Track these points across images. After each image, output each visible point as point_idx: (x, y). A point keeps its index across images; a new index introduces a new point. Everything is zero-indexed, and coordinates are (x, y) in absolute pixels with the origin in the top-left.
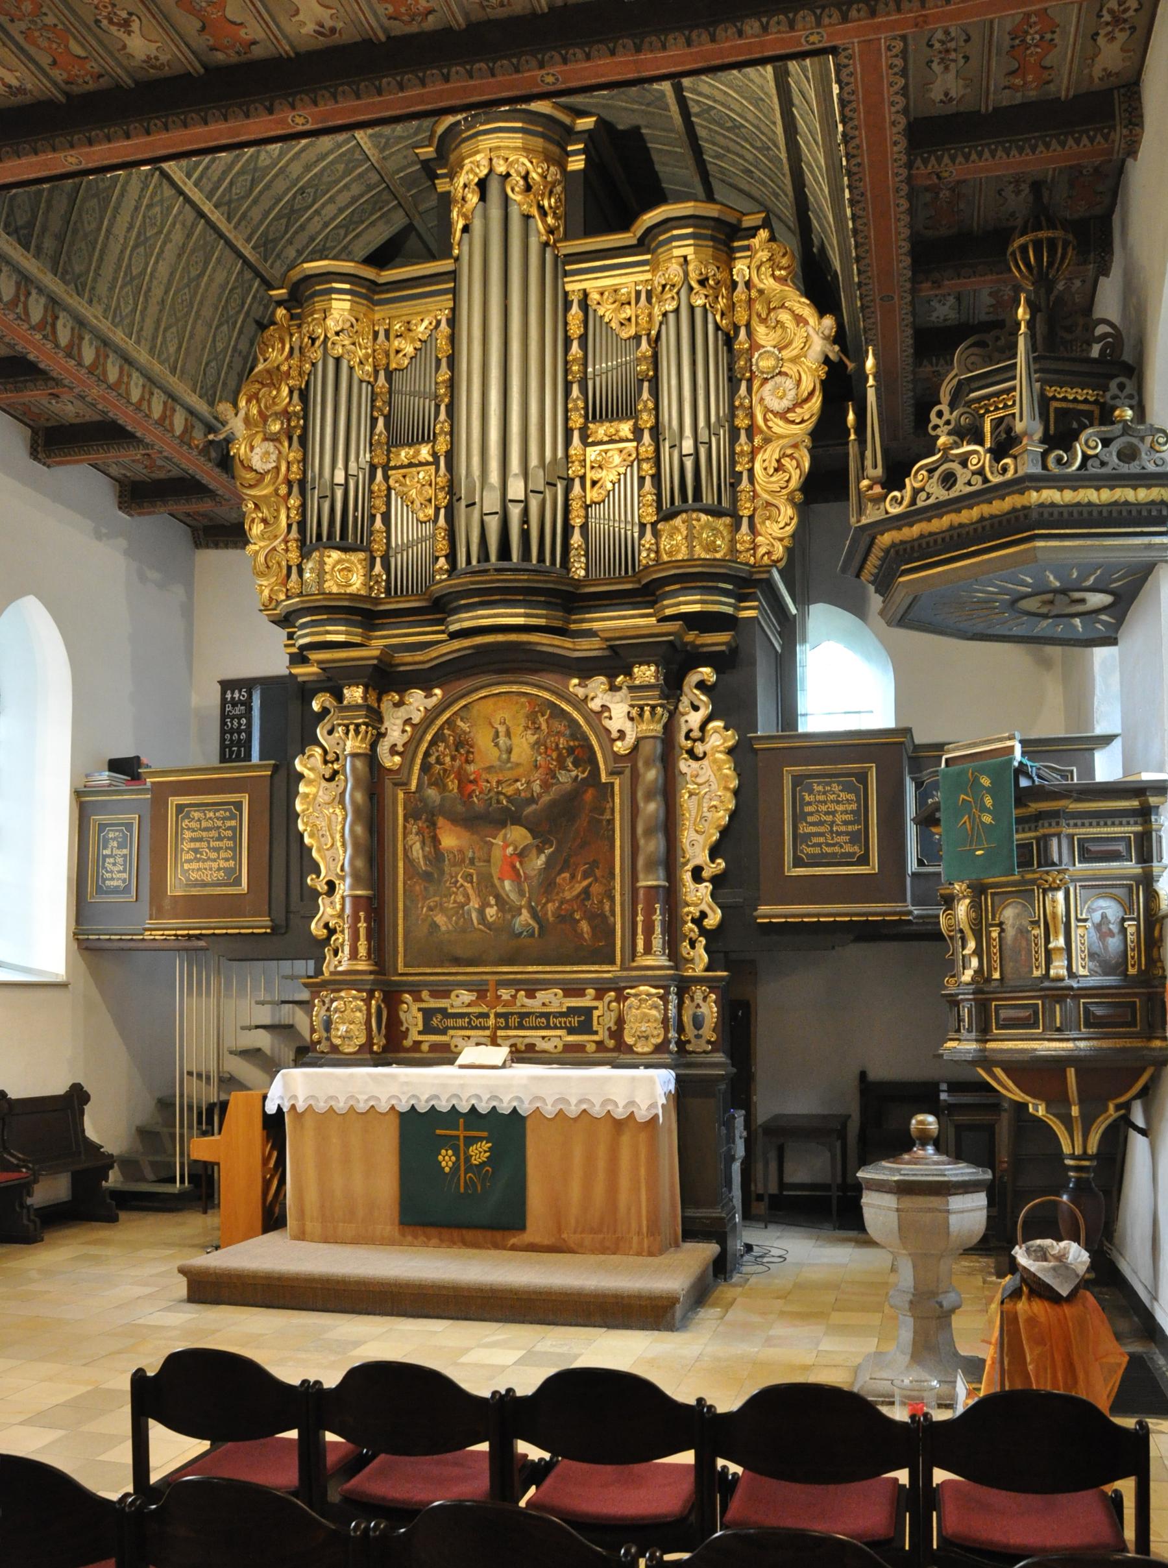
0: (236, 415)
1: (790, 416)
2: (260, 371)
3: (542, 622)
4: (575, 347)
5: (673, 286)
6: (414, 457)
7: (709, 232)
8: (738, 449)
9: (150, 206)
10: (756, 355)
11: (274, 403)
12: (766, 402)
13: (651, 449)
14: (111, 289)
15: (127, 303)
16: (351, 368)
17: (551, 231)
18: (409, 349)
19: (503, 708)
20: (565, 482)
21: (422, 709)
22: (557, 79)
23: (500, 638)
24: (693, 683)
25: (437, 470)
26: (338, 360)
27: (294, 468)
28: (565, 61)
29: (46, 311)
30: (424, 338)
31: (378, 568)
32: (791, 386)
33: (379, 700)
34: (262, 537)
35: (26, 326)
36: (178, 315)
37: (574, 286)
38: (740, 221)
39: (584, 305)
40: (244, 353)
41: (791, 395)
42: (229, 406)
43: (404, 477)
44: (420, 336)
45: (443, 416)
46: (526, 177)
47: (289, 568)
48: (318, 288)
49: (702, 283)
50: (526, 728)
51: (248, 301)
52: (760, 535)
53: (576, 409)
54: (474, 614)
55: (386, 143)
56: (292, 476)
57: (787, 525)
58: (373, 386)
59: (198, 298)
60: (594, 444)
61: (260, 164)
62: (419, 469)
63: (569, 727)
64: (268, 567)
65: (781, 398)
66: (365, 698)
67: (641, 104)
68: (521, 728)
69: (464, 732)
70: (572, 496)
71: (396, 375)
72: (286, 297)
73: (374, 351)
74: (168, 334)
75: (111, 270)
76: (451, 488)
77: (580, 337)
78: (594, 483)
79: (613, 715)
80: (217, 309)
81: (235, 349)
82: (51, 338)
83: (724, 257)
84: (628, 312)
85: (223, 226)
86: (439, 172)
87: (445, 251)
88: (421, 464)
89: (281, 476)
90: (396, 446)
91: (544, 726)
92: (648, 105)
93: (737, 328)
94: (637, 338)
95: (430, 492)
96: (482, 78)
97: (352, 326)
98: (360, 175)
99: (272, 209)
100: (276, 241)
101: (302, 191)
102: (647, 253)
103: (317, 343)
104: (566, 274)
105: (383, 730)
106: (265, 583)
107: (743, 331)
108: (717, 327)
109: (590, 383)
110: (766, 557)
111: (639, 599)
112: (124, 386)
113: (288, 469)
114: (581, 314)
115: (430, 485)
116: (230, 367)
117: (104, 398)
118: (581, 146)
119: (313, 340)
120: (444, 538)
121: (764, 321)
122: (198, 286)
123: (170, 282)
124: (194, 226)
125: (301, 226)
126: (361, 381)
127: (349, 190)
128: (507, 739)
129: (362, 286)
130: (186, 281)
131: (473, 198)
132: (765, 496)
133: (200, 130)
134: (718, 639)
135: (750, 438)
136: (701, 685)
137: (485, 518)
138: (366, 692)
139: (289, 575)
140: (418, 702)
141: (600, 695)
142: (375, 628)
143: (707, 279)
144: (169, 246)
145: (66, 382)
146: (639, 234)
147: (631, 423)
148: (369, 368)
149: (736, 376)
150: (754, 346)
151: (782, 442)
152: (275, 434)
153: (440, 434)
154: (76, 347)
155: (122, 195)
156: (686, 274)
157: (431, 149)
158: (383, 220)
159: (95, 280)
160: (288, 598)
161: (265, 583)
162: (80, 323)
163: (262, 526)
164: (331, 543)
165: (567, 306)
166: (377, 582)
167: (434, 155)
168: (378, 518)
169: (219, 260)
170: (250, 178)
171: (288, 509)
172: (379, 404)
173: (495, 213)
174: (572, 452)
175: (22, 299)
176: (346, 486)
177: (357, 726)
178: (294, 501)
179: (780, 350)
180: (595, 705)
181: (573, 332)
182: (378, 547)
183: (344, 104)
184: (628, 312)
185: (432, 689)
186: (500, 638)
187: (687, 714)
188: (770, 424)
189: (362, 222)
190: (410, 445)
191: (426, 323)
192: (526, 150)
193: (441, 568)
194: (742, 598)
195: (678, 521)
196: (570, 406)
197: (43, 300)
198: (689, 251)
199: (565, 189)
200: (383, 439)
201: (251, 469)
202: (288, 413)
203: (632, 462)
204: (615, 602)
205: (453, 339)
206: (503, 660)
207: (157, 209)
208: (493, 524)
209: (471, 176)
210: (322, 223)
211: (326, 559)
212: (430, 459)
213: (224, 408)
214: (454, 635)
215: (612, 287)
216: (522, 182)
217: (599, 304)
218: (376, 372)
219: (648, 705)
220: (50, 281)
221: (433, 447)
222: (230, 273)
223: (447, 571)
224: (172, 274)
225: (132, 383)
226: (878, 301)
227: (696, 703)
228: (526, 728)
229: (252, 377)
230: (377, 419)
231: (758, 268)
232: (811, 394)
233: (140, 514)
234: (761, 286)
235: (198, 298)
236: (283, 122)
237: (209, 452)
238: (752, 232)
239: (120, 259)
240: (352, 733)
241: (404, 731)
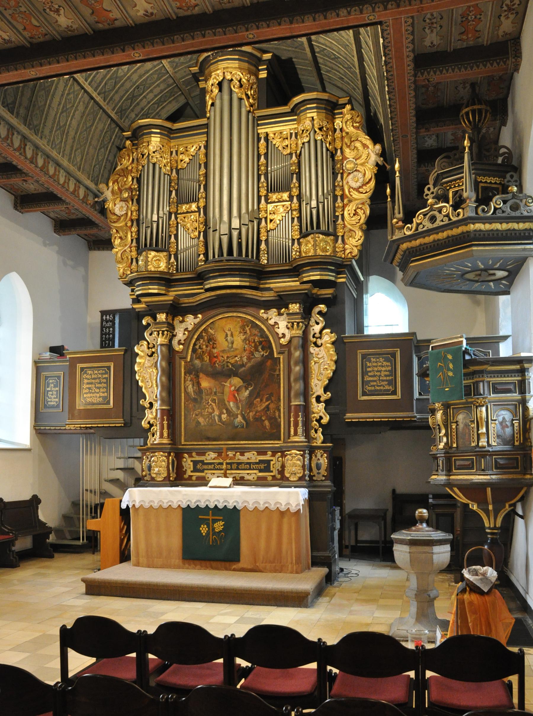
0: (108, 189)
1: (361, 190)
2: (119, 170)
3: (247, 284)
4: (262, 159)
5: (307, 130)
6: (189, 209)
7: (324, 106)
8: (337, 205)
9: (68, 94)
10: (345, 162)
11: (125, 184)
12: (349, 184)
13: (297, 205)
15: (58, 138)
16: (160, 168)
17: (251, 105)
19: (230, 323)
20: (258, 220)
21: (193, 324)
22: (254, 36)
23: (228, 291)
24: (316, 312)
25: (200, 215)
26: (154, 164)
27: (134, 214)
28: (258, 28)
29: (21, 142)
30: (193, 154)
31: (172, 259)
32: (361, 176)
33: (173, 320)
34: (120, 245)
35: (12, 149)
36: (81, 144)
37: (262, 131)
38: (338, 101)
39: (267, 139)
40: (112, 161)
41: (361, 180)
42: (104, 185)
43: (184, 218)
44: (192, 153)
45: (202, 190)
46: (240, 81)
47: (132, 259)
48: (145, 131)
49: (321, 129)
50: (240, 332)
51: (113, 138)
52: (347, 244)
53: (263, 187)
54: (216, 280)
55: (176, 65)
56: (133, 218)
57: (359, 240)
58: (170, 176)
59: (91, 136)
60: (271, 203)
61: (119, 75)
62: (191, 214)
64: (122, 259)
65: (357, 182)
66: (166, 319)
67: (293, 47)
68: (238, 332)
69: (212, 334)
70: (261, 226)
71: (181, 171)
72: (130, 136)
73: (171, 160)
74: (77, 152)
75: (51, 123)
76: (206, 223)
77: (265, 154)
78: (271, 221)
79: (280, 326)
80: (99, 141)
81: (107, 159)
82: (23, 154)
83: (330, 117)
84: (287, 142)
85: (102, 103)
86: (200, 78)
87: (203, 115)
88: (192, 212)
89: (128, 218)
90: (181, 204)
91: (248, 332)
92: (296, 48)
93: (336, 150)
94: (291, 154)
95: (196, 225)
96: (220, 36)
97: (161, 149)
98: (164, 80)
99: (124, 95)
100: (126, 110)
101: (138, 87)
102: (295, 115)
103: (145, 157)
104: (258, 125)
105: (175, 333)
106: (121, 266)
107: (339, 151)
109: (269, 175)
110: (349, 255)
111: (292, 274)
112: (56, 176)
113: (132, 214)
114: (265, 144)
115: (196, 221)
116: (105, 167)
117: (47, 182)
118: (265, 67)
119: (143, 155)
120: (202, 246)
121: (348, 147)
122: (90, 130)
123: (78, 129)
124: (88, 103)
125: (137, 103)
126: (165, 174)
127: (159, 87)
129: (165, 131)
130: (85, 128)
131: (216, 91)
132: (349, 226)
134: (328, 292)
135: (342, 200)
136: (320, 313)
137: (221, 236)
138: (167, 316)
139: (132, 263)
140: (191, 321)
141: (274, 317)
142: (171, 287)
143: (323, 127)
144: (77, 112)
145: (30, 174)
146: (291, 107)
147: (288, 193)
148: (168, 168)
149: (336, 172)
150: (344, 158)
151: (357, 202)
152: (126, 198)
153: (201, 198)
154: (34, 159)
155: (56, 89)
156: (313, 125)
157: (197, 68)
158: (175, 100)
159: (43, 128)
160: (131, 273)
161: (121, 266)
162: (37, 147)
163: (120, 240)
164: (151, 248)
165: (259, 140)
167: (198, 71)
168: (173, 236)
169: (100, 119)
171: (132, 232)
172: (173, 184)
173: (226, 97)
174: (261, 206)
175: (10, 136)
176: (158, 222)
177: (163, 331)
178: (134, 229)
179: (356, 160)
180: (271, 322)
182: (173, 250)
184: (287, 142)
185: (197, 314)
186: (228, 291)
187: (314, 326)
188: (351, 193)
189: (165, 101)
190: (187, 203)
191: (194, 147)
192: (240, 68)
193: (201, 260)
194: (338, 273)
195: (309, 238)
197: (19, 137)
198: (314, 115)
199: (258, 86)
200: (175, 200)
202: (132, 189)
203: (289, 211)
204: (280, 275)
205: (207, 155)
206: (230, 301)
207: (72, 96)
208: (225, 239)
209: (215, 81)
210: (147, 102)
211: (149, 255)
212: (196, 210)
213: (102, 186)
214: (207, 290)
215: (279, 131)
216: (238, 83)
217: (273, 139)
218: (172, 170)
219: (296, 322)
220: (23, 128)
221: (198, 204)
222: (105, 125)
223: (204, 261)
224: (78, 125)
225: (60, 175)
227: (318, 321)
228: (240, 332)
229: (115, 172)
230: (172, 191)
231: (346, 122)
232: (370, 180)
233: (64, 235)
234: (347, 131)
235: (91, 136)
238: (343, 106)
239: (55, 118)
240: (160, 335)
241: (184, 334)
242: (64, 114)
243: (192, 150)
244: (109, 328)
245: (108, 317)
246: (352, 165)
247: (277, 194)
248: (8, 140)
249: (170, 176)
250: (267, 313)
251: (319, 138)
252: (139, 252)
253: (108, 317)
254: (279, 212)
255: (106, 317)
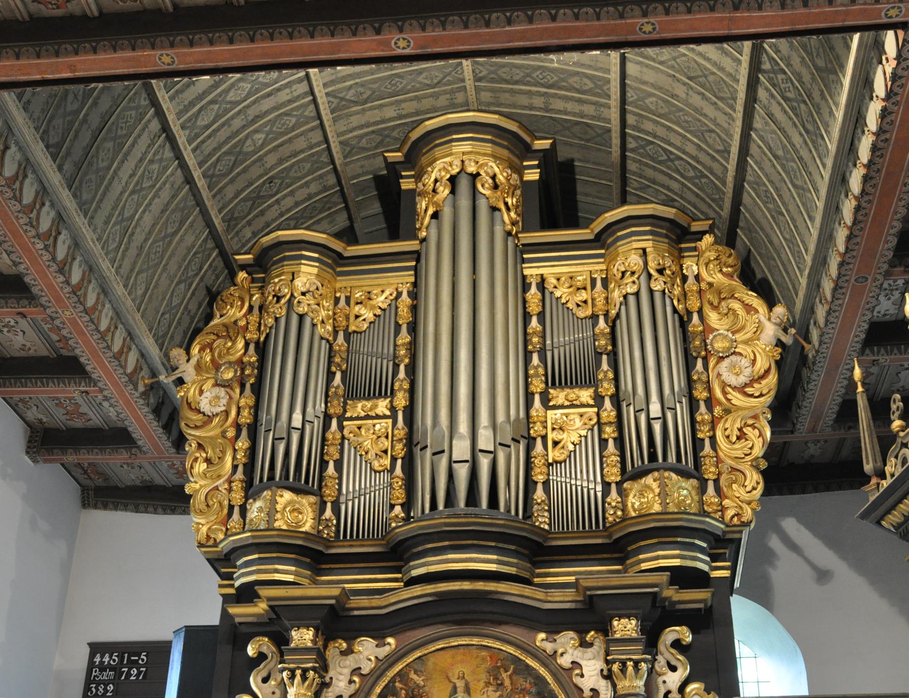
0: (188, 361)
1: (749, 390)
2: (215, 325)
3: (512, 570)
4: (534, 322)
5: (633, 273)
6: (371, 409)
7: (664, 232)
8: (699, 418)
9: (151, 162)
10: (711, 337)
11: (228, 353)
12: (723, 378)
13: (614, 413)
14: (107, 223)
15: (114, 240)
16: (314, 325)
17: (514, 223)
18: (368, 315)
19: (462, 662)
20: (526, 441)
21: (373, 658)
22: (654, 29)
23: (466, 585)
24: (669, 642)
25: (395, 423)
26: (301, 317)
27: (245, 413)
28: (667, 12)
29: (52, 225)
30: (384, 306)
31: (328, 513)
32: (747, 364)
33: (325, 647)
34: (204, 475)
35: (33, 233)
36: (151, 264)
37: (532, 271)
38: (689, 225)
39: (542, 285)
40: (192, 313)
41: (747, 372)
42: (182, 352)
43: (359, 428)
44: (380, 305)
45: (402, 374)
46: (494, 177)
47: (231, 508)
48: (287, 254)
49: (661, 271)
50: (488, 684)
51: (206, 267)
52: (727, 497)
53: (537, 375)
54: (445, 557)
55: (350, 152)
56: (242, 420)
57: (754, 489)
58: (331, 345)
59: (168, 253)
60: (555, 407)
61: (245, 149)
62: (376, 421)
63: (536, 684)
64: (208, 506)
65: (737, 374)
66: (314, 642)
67: (581, 139)
68: (482, 684)
69: (418, 685)
70: (534, 453)
71: (354, 338)
72: (252, 262)
73: (335, 314)
74: (140, 277)
75: (109, 207)
76: (410, 441)
77: (538, 314)
78: (556, 443)
79: (584, 672)
80: (180, 267)
81: (186, 308)
82: (51, 249)
83: (676, 253)
84: (584, 295)
85: (205, 194)
86: (403, 174)
87: (412, 234)
88: (378, 417)
89: (230, 420)
90: (352, 399)
91: (507, 682)
92: (588, 141)
93: (689, 313)
94: (594, 317)
95: (387, 444)
96: (587, 20)
97: (317, 289)
98: (321, 177)
99: (243, 190)
100: (238, 220)
101: (271, 180)
102: (601, 248)
103: (283, 301)
104: (524, 261)
105: (327, 680)
106: (203, 521)
107: (695, 317)
108: (675, 310)
109: (549, 354)
110: (735, 519)
111: (605, 556)
112: (97, 313)
113: (238, 413)
114: (539, 295)
115: (387, 437)
116: (179, 323)
117: (74, 322)
118: (536, 163)
119: (279, 299)
120: (401, 487)
121: (715, 308)
122: (170, 242)
123: (150, 233)
124: (180, 189)
125: (261, 211)
126: (322, 338)
127: (308, 187)
128: (466, 695)
129: (329, 257)
130: (163, 234)
131: (444, 191)
132: (730, 462)
133: (307, 42)
134: (696, 596)
135: (710, 409)
136: (677, 644)
137: (455, 465)
138: (316, 635)
139: (230, 514)
140: (368, 651)
141: (570, 651)
142: (320, 572)
143: (664, 269)
144: (157, 200)
145: (43, 300)
146: (597, 231)
147: (591, 391)
148: (330, 328)
149: (693, 352)
150: (708, 329)
151: (746, 413)
152: (227, 381)
153: (399, 390)
154: (68, 265)
155: (133, 145)
156: (646, 263)
157: (400, 154)
158: (328, 220)
159: (95, 211)
160: (227, 535)
161: (203, 521)
162: (76, 244)
163: (204, 466)
164: (285, 483)
165: (526, 287)
166: (327, 526)
167: (402, 159)
168: (331, 465)
169: (191, 225)
170: (233, 158)
171: (235, 450)
172: (337, 360)
173: (464, 203)
174: (533, 413)
175: (38, 206)
176: (302, 430)
177: (305, 671)
178: (243, 444)
179: (733, 333)
180: (565, 661)
181: (532, 313)
182: (329, 493)
183: (451, 32)
184: (584, 295)
185: (385, 637)
186: (466, 585)
187: (664, 674)
188: (729, 396)
189: (311, 218)
190: (369, 398)
191: (387, 293)
192: (495, 157)
193: (397, 516)
194: (714, 558)
195: (649, 480)
196: (531, 372)
197: (53, 214)
198: (648, 245)
199: (522, 194)
200: (341, 392)
201: (199, 412)
202: (243, 363)
203: (593, 426)
204: (580, 557)
205: (414, 309)
206: (465, 610)
207: (155, 166)
208: (462, 472)
209: (443, 173)
210: (279, 212)
211: (278, 499)
212: (388, 413)
213: (177, 353)
214: (412, 582)
215: (564, 276)
216: (490, 181)
217: (555, 287)
218: (336, 332)
219: (630, 660)
220: (65, 197)
221: (391, 402)
222: (197, 238)
223: (403, 519)
224: (154, 225)
225: (103, 314)
226: (853, 281)
227: (673, 663)
228: (488, 684)
229: (208, 329)
230: (334, 373)
231: (707, 265)
232: (767, 372)
233: (45, 461)
234: (710, 280)
235: (168, 253)
236: (387, 43)
237: (149, 396)
238: (699, 235)
239: (119, 199)
240: (298, 678)
241: (351, 682)
242: (136, 197)
243: (382, 298)
244: (106, 685)
245: (106, 659)
246: (727, 344)
247: (568, 390)
248: (32, 212)
249: (331, 345)
250: (555, 640)
251: (657, 286)
252: (251, 490)
253: (106, 659)
254: (570, 422)
255: (102, 657)
